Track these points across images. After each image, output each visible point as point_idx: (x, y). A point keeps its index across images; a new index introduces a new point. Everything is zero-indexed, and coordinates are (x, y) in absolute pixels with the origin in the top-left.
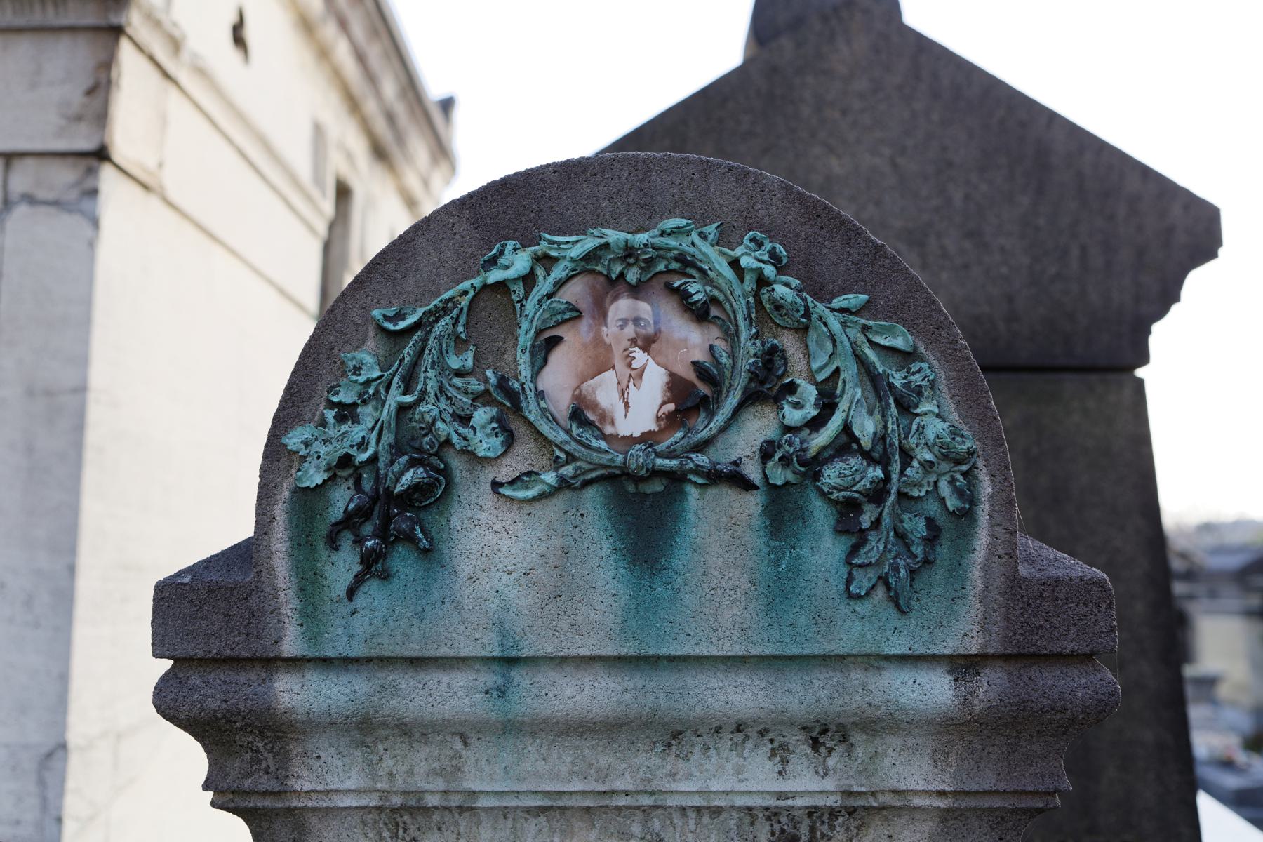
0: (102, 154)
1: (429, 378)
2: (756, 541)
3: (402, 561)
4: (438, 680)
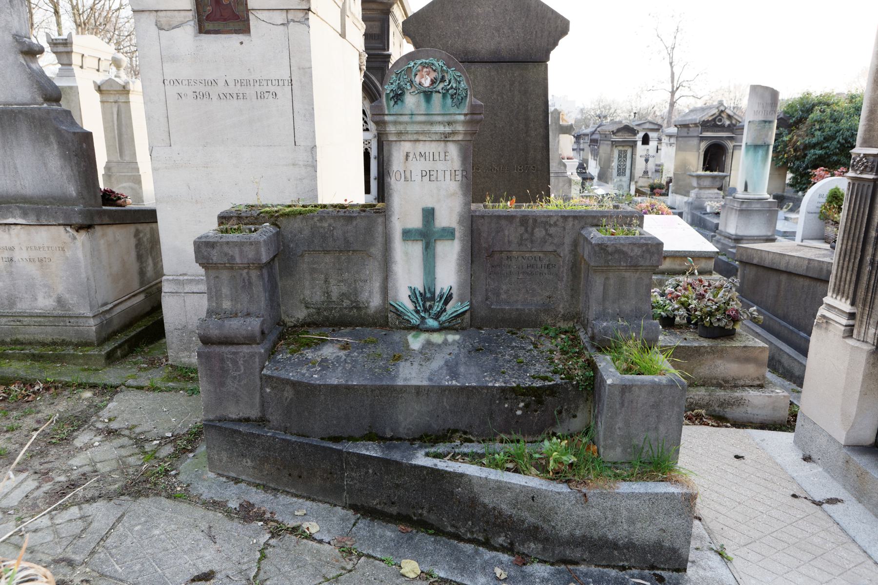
0: (309, 10)
1: (402, 79)
2: (441, 99)
3: (399, 102)
4: (404, 117)
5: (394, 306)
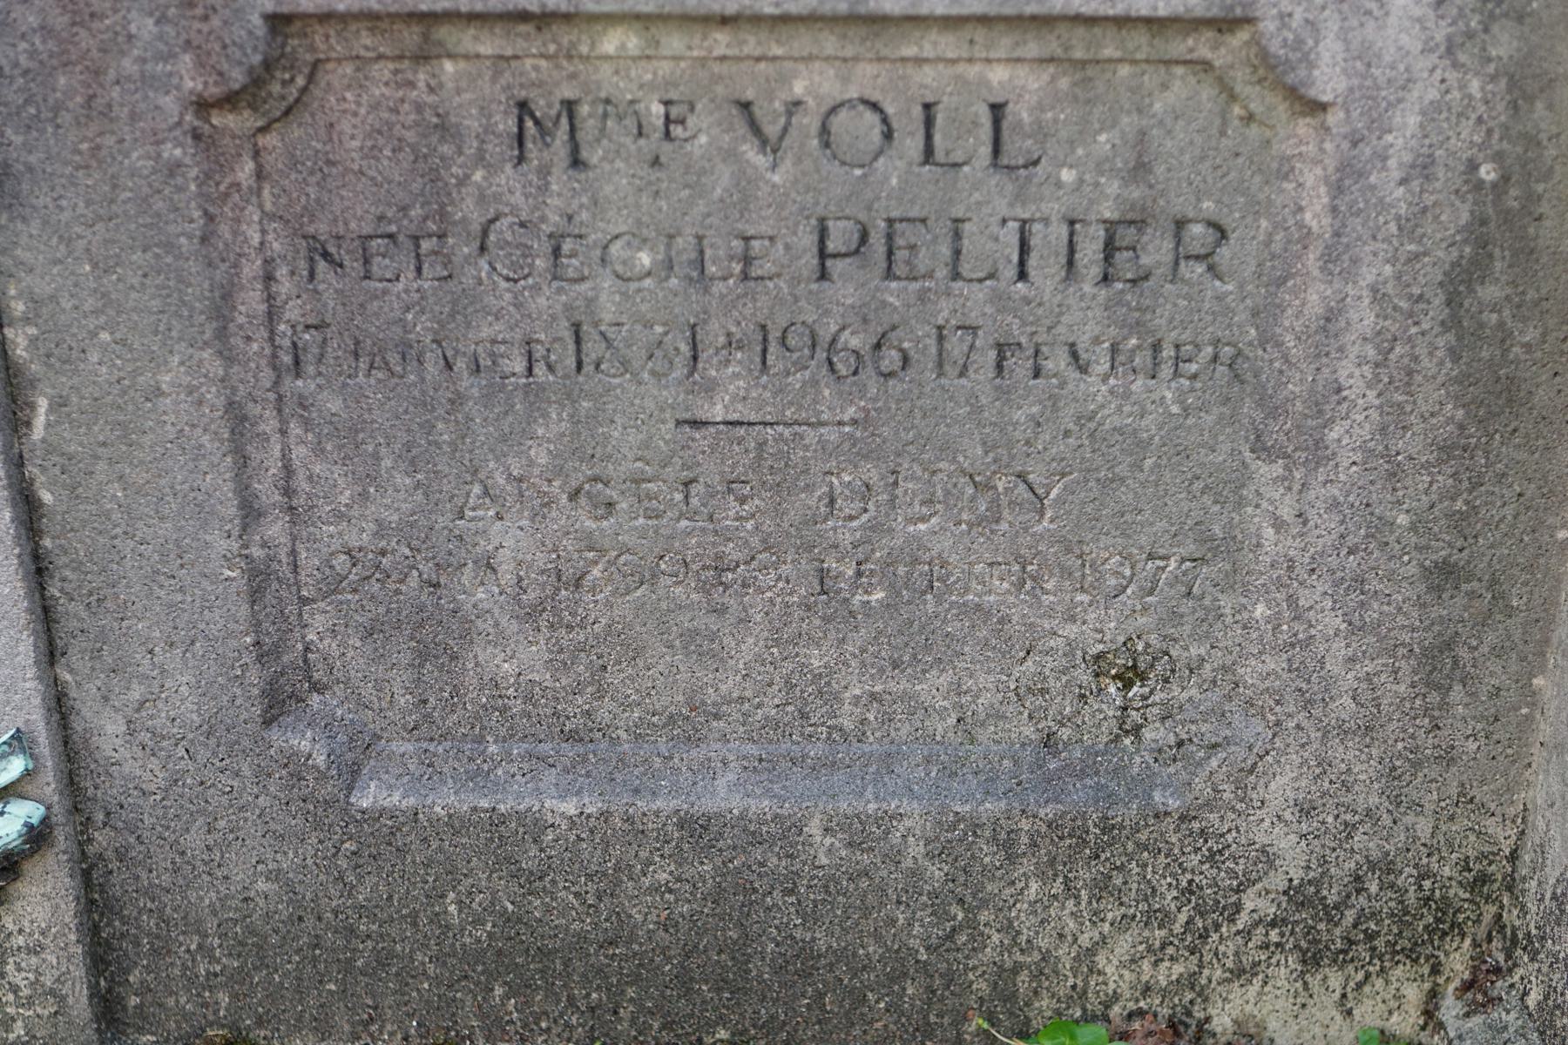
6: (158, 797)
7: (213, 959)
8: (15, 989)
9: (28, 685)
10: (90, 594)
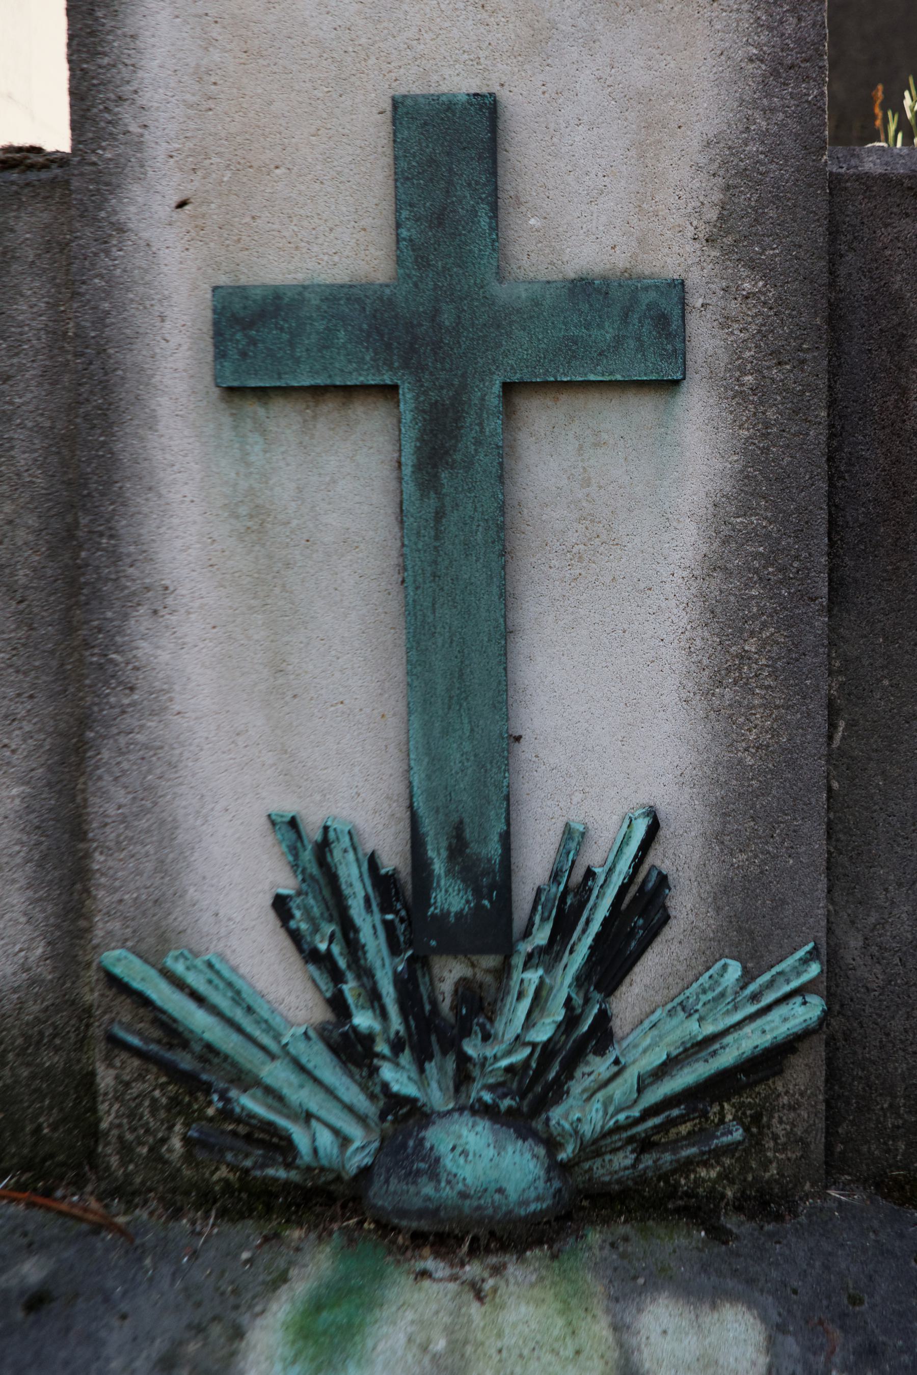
5: (143, 1001)
6: (877, 993)
7: (899, 1116)
8: (775, 1137)
9: (819, 912)
10: (853, 849)
